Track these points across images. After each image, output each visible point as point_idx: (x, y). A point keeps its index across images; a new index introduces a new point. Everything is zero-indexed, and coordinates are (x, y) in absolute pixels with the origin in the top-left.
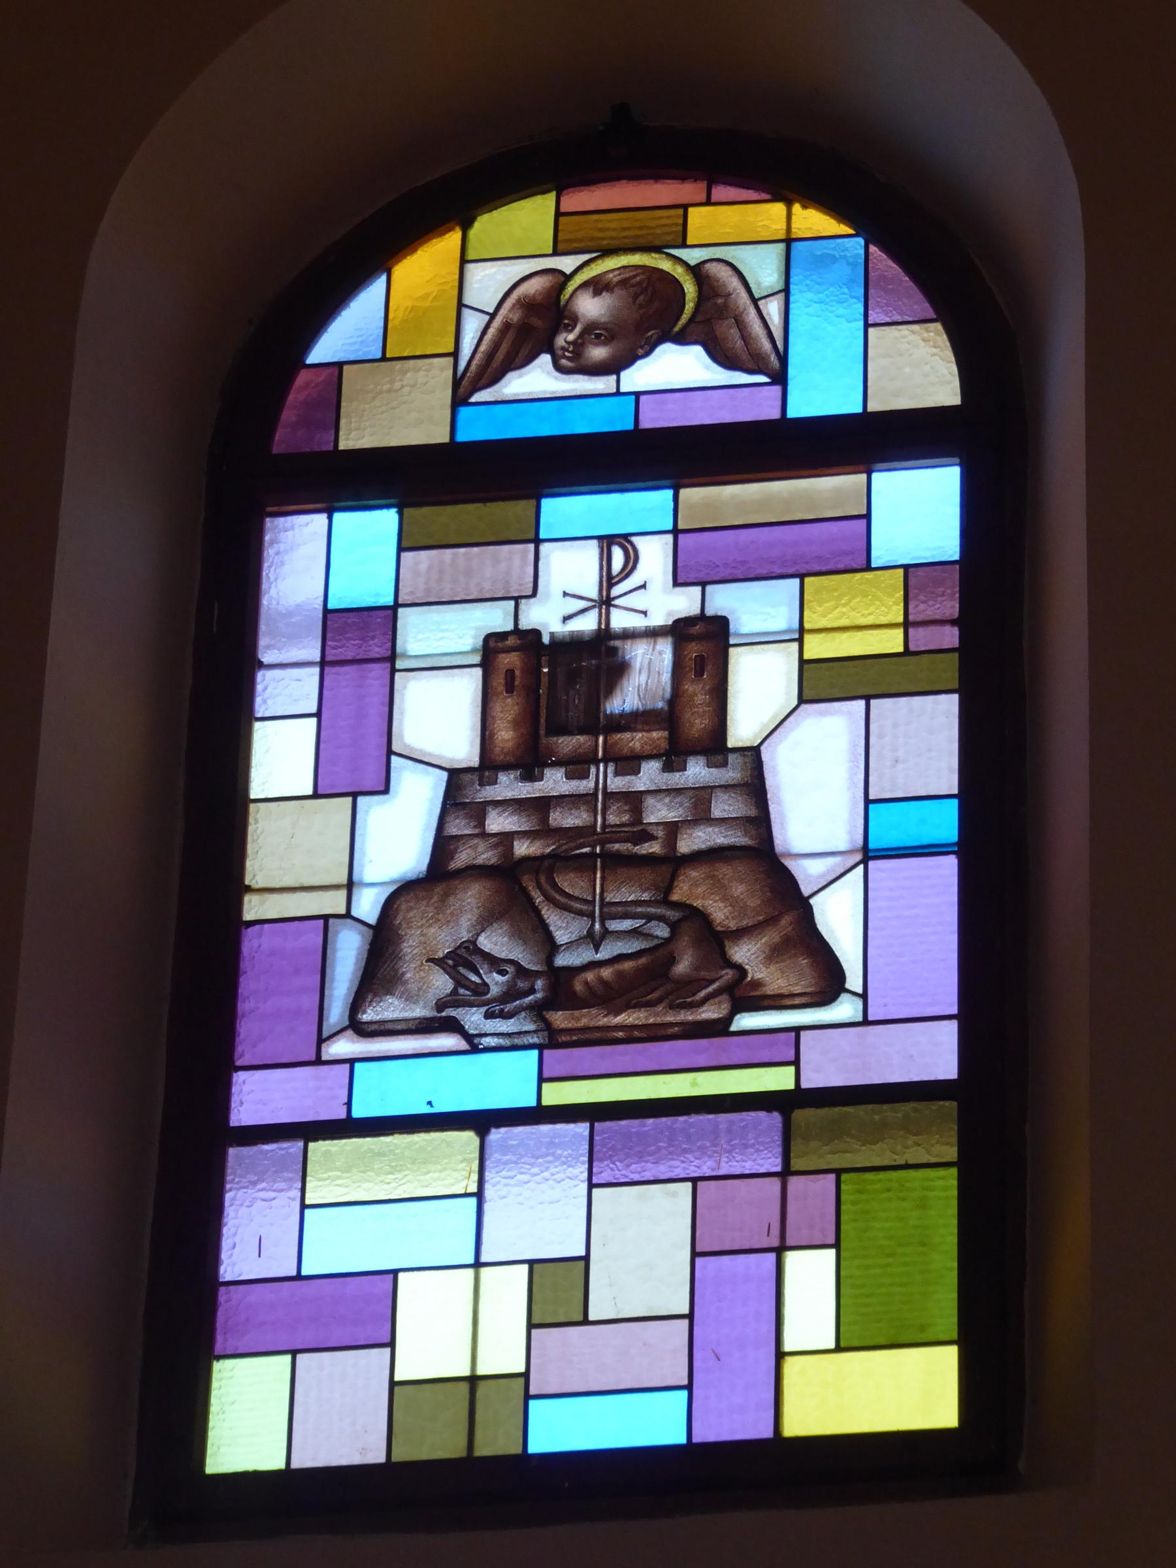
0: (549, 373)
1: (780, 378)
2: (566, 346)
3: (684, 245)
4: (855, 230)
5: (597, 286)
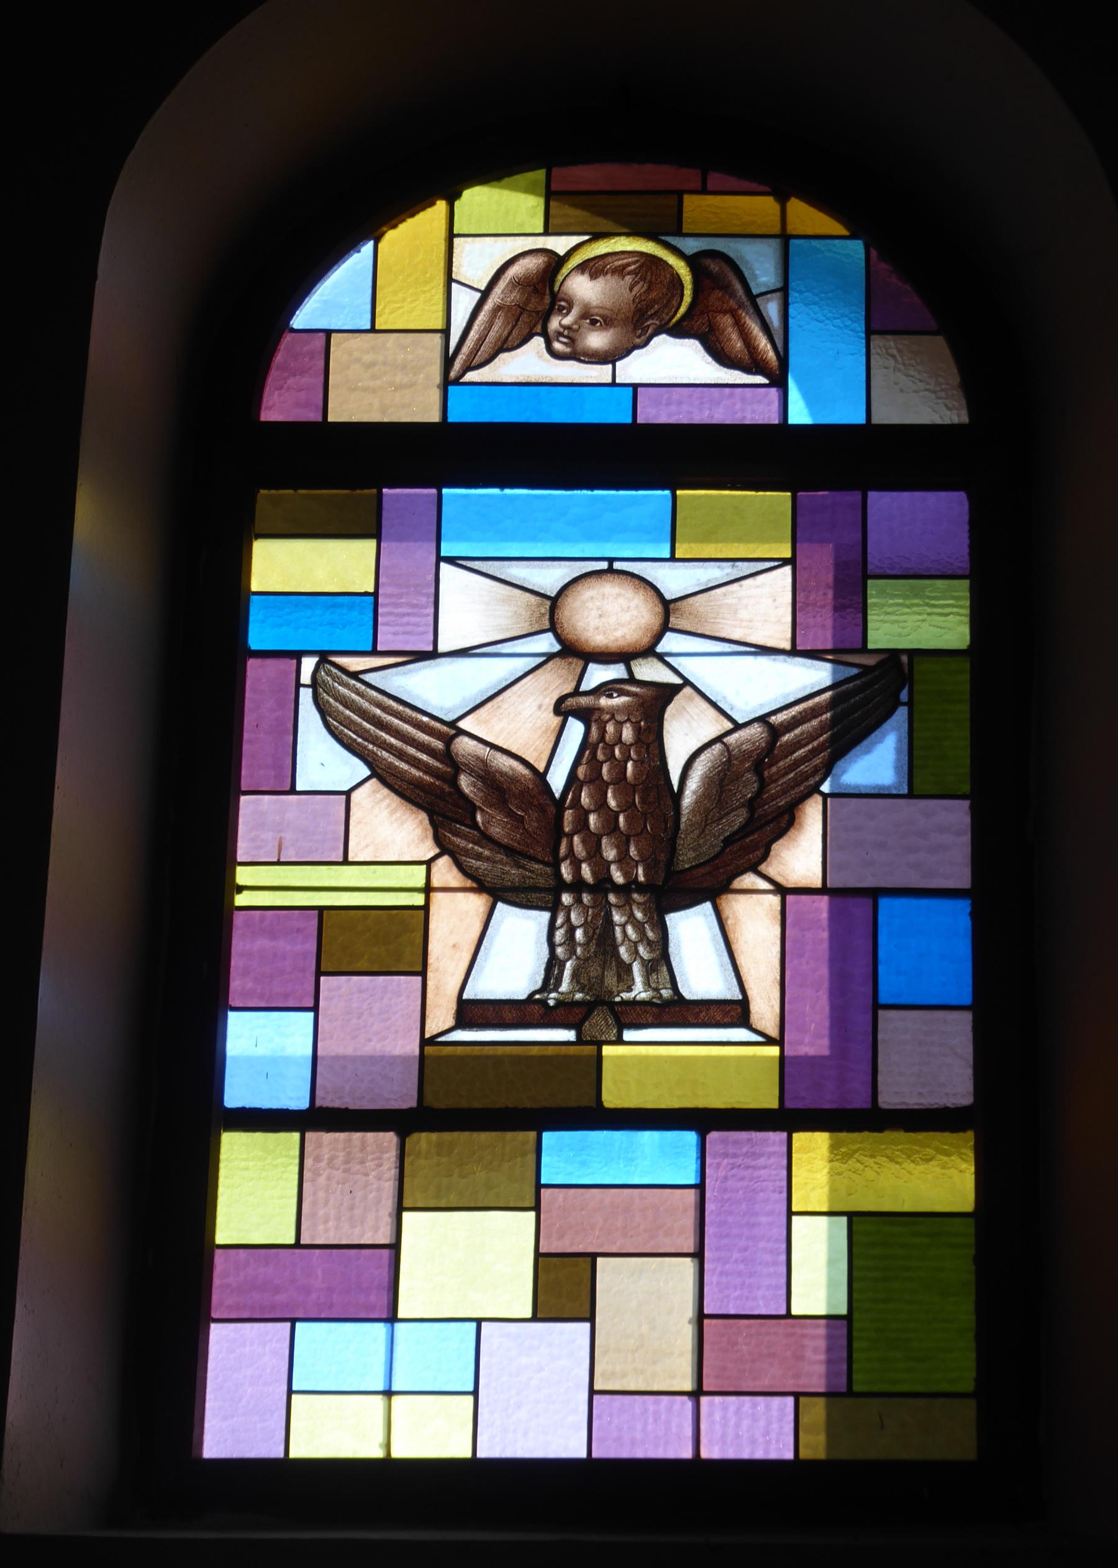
0: (540, 357)
1: (779, 380)
2: (562, 330)
3: (679, 233)
4: (847, 227)
5: (593, 268)
